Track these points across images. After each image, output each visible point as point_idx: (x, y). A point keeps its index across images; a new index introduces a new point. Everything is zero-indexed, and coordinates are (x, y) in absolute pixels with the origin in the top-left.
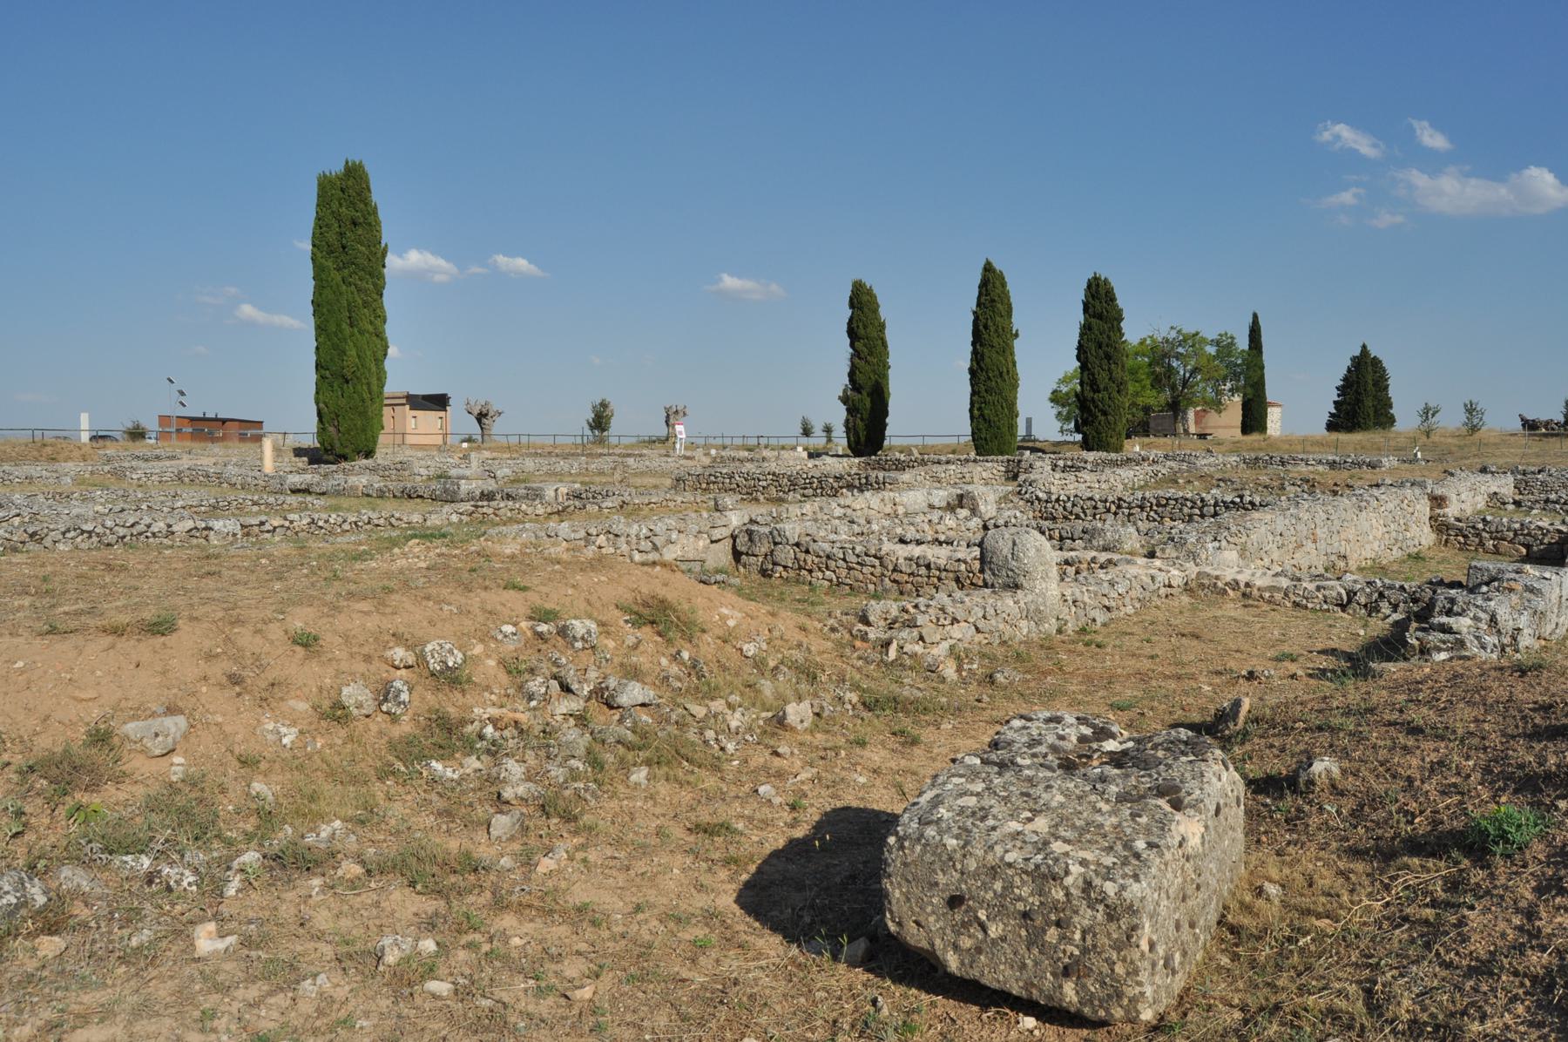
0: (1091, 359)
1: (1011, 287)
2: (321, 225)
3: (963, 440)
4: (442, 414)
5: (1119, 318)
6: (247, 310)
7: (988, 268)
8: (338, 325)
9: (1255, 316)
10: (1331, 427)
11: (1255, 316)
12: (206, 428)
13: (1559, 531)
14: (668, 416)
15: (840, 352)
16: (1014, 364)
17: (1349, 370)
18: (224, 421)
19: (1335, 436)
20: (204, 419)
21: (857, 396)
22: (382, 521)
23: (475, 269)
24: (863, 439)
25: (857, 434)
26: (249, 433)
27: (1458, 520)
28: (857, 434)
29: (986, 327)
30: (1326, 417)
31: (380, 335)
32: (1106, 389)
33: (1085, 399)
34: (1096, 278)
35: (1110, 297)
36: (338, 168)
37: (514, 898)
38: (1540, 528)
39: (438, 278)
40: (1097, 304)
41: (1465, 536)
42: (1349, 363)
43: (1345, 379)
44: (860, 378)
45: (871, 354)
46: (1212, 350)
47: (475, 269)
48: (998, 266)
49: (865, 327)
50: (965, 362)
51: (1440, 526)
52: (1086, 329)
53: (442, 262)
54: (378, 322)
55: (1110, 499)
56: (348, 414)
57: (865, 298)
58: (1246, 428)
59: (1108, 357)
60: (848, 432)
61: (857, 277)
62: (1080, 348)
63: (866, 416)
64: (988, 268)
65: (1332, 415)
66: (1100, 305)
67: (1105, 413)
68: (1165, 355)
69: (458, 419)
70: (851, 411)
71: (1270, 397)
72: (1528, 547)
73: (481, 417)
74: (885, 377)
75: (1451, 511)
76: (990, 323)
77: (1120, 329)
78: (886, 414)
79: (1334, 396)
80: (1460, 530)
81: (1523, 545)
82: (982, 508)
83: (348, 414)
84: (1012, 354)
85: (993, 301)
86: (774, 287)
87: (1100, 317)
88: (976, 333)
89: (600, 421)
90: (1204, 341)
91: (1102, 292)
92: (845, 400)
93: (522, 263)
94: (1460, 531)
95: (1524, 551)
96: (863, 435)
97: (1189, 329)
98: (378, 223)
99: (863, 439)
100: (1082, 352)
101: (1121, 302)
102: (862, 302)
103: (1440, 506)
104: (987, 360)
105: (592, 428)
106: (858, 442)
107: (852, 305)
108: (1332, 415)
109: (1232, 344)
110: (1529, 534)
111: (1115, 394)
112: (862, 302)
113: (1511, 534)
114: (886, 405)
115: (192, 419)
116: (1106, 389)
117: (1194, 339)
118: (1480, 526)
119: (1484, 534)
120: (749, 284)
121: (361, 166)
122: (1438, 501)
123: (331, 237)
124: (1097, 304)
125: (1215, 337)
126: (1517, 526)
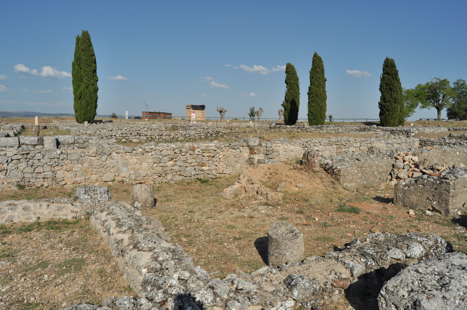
3: (305, 120)
4: (203, 111)
6: (214, 83)
7: (315, 55)
12: (154, 115)
15: (283, 88)
18: (160, 113)
20: (155, 113)
23: (275, 70)
26: (168, 116)
37: (60, 300)
39: (265, 73)
46: (452, 86)
47: (275, 70)
48: (319, 54)
52: (383, 79)
53: (265, 68)
59: (390, 89)
61: (288, 62)
63: (289, 111)
66: (390, 72)
67: (388, 110)
68: (435, 89)
73: (221, 112)
78: (298, 111)
83: (86, 110)
86: (365, 72)
87: (388, 74)
96: (287, 117)
97: (443, 79)
99: (287, 119)
105: (250, 116)
106: (286, 121)
107: (286, 72)
111: (393, 103)
115: (150, 113)
120: (358, 72)
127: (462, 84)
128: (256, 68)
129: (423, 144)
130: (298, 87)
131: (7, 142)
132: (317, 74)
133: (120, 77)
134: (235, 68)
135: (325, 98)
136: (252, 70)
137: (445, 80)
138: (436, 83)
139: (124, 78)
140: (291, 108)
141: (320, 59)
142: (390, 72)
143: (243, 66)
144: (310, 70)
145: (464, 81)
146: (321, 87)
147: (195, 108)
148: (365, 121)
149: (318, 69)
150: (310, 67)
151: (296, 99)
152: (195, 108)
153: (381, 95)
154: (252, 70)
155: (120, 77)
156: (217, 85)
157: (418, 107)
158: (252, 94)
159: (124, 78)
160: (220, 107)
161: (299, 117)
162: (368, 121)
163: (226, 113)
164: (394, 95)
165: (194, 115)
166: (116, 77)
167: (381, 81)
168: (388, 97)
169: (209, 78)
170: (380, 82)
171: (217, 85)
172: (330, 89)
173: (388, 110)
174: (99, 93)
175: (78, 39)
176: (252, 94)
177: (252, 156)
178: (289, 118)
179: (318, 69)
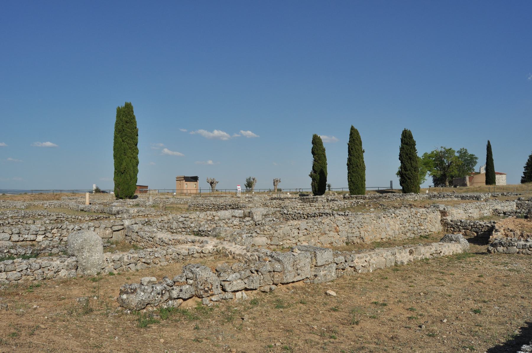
0: (404, 159)
1: (361, 134)
2: (117, 124)
4: (196, 183)
5: (414, 144)
6: (166, 150)
7: (352, 128)
8: (120, 155)
9: (489, 142)
10: (523, 182)
11: (489, 142)
13: (488, 226)
14: (274, 183)
15: (310, 159)
16: (363, 162)
17: (529, 160)
19: (524, 185)
21: (315, 175)
22: (14, 223)
23: (236, 135)
24: (317, 190)
25: (315, 188)
27: (452, 221)
28: (315, 188)
29: (352, 149)
30: (520, 179)
31: (136, 158)
32: (410, 170)
33: (403, 174)
34: (405, 130)
35: (411, 137)
36: (122, 105)
38: (480, 225)
39: (225, 139)
40: (406, 139)
41: (454, 228)
42: (528, 158)
43: (527, 164)
44: (315, 168)
45: (319, 160)
46: (457, 155)
47: (236, 135)
48: (355, 127)
49: (317, 150)
50: (346, 162)
51: (444, 223)
52: (402, 149)
53: (225, 134)
54: (134, 154)
55: (305, 213)
56: (126, 184)
57: (317, 140)
58: (487, 183)
59: (410, 158)
60: (312, 187)
61: (314, 133)
62: (400, 155)
64: (352, 128)
65: (523, 177)
66: (407, 141)
67: (409, 179)
68: (441, 157)
69: (203, 184)
70: (314, 180)
71: (496, 171)
72: (477, 232)
73: (211, 183)
74: (325, 168)
75: (449, 218)
76: (353, 148)
77: (414, 148)
79: (523, 170)
80: (452, 225)
81: (475, 232)
82: (255, 217)
83: (126, 184)
84: (362, 158)
85: (354, 140)
86: (333, 138)
87: (407, 144)
88: (349, 152)
89: (249, 185)
90: (454, 151)
91: (407, 135)
92: (311, 176)
93: (249, 132)
94: (452, 226)
95: (476, 234)
96: (317, 188)
97: (448, 148)
98: (136, 122)
99: (317, 190)
100: (401, 158)
101: (415, 138)
102: (317, 142)
103: (444, 216)
104: (352, 161)
106: (315, 191)
107: (313, 143)
108: (523, 177)
109: (466, 152)
110: (476, 227)
111: (413, 172)
112: (317, 142)
113: (470, 227)
114: (326, 178)
116: (410, 170)
117: (449, 151)
118: (459, 224)
119: (460, 227)
121: (130, 104)
122: (444, 213)
123: (120, 127)
124: (406, 139)
125: (459, 150)
126: (472, 224)
127: (465, 153)
128: (216, 132)
129: (520, 206)
130: (325, 157)
131: (225, 215)
132: (356, 146)
133: (49, 144)
134: (192, 133)
135: (364, 169)
136: (211, 134)
137: (450, 149)
138: (441, 152)
139: (55, 145)
140: (320, 179)
141: (357, 131)
142: (407, 141)
143: (201, 131)
144: (348, 142)
145: (466, 150)
146: (360, 158)
147: (188, 179)
148: (377, 189)
149: (357, 141)
150: (347, 139)
151: (324, 169)
152: (188, 179)
153: (400, 164)
154: (211, 134)
155: (49, 144)
156: (170, 152)
157: (427, 176)
158: (210, 162)
159: (55, 145)
160: (211, 177)
161: (367, 185)
162: (380, 189)
163: (217, 184)
164: (414, 164)
165: (190, 186)
166: (44, 143)
167: (401, 151)
168: (408, 166)
169: (161, 145)
170: (399, 151)
171: (170, 152)
172: (368, 159)
173: (409, 179)
174: (139, 167)
175: (119, 111)
176: (210, 162)
177: (445, 218)
178: (319, 189)
179: (357, 141)
